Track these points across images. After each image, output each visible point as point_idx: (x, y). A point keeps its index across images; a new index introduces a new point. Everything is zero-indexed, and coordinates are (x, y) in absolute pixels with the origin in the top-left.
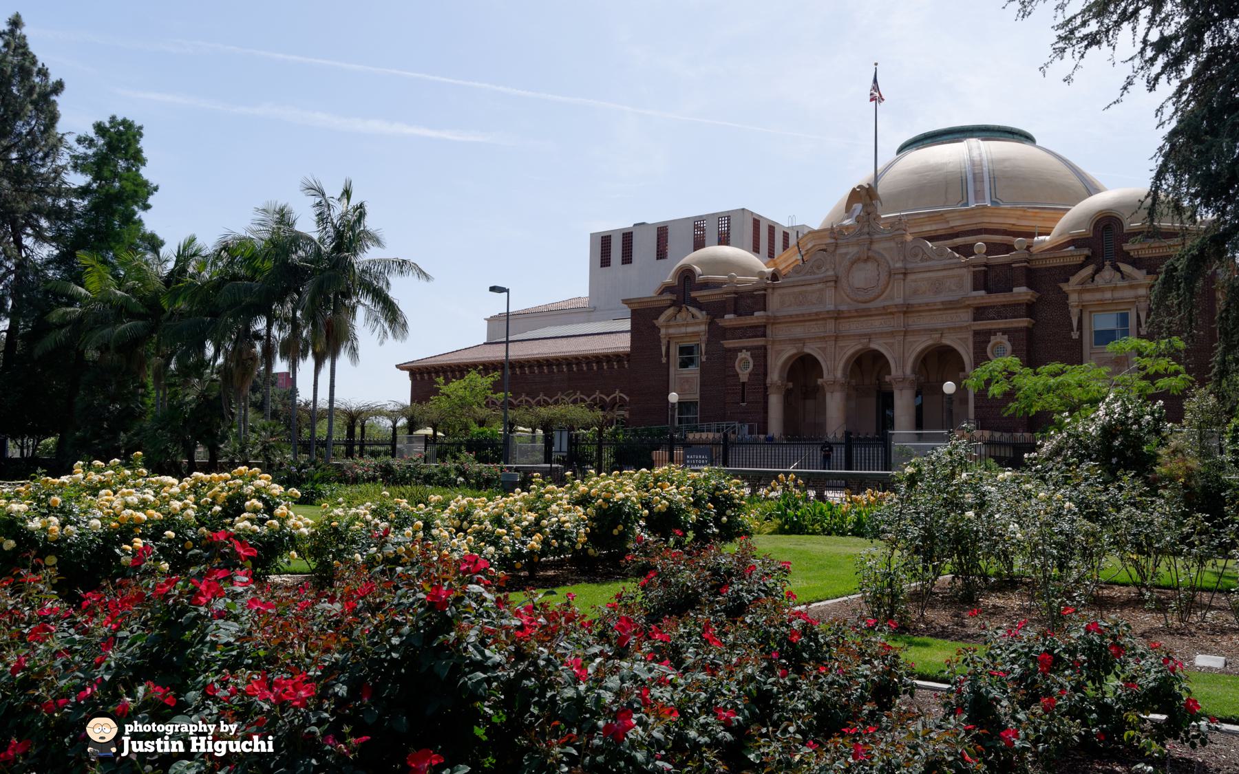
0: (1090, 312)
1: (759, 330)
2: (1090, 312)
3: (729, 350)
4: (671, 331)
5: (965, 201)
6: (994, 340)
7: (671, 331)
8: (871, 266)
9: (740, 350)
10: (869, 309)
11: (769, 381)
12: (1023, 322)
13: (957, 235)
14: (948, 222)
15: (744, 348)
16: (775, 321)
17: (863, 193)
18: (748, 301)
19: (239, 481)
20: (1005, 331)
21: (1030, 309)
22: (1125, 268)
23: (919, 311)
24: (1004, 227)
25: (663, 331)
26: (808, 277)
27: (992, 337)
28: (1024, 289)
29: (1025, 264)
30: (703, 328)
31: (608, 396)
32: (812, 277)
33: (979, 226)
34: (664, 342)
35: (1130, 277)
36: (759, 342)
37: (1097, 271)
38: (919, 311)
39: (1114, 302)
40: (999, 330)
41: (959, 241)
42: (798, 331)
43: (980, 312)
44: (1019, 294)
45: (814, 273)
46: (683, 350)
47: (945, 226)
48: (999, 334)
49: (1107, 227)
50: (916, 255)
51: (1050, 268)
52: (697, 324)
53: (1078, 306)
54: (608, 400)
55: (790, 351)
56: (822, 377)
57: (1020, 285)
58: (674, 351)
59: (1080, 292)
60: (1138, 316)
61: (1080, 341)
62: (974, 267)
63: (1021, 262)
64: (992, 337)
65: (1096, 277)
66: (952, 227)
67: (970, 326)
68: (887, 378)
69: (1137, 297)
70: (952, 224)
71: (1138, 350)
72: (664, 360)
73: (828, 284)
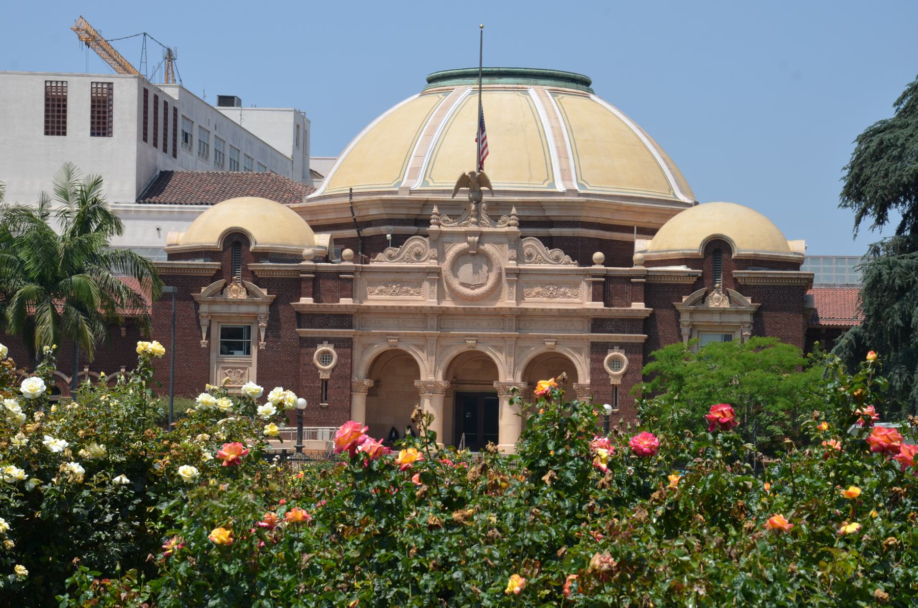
0: (699, 331)
1: (344, 319)
2: (699, 331)
4: (217, 308)
5: (550, 181)
7: (217, 308)
9: (321, 341)
13: (550, 223)
14: (544, 210)
15: (325, 339)
17: (473, 181)
19: (166, 442)
20: (622, 346)
21: (646, 324)
24: (600, 221)
25: (204, 309)
29: (644, 280)
30: (264, 309)
33: (576, 219)
39: (721, 325)
40: (617, 344)
41: (555, 231)
43: (598, 323)
45: (413, 261)
46: (227, 333)
47: (542, 214)
51: (664, 285)
52: (257, 304)
53: (688, 326)
57: (639, 301)
58: (216, 333)
59: (692, 313)
62: (593, 277)
63: (640, 278)
66: (548, 216)
69: (742, 323)
70: (548, 213)
71: (47, 215)
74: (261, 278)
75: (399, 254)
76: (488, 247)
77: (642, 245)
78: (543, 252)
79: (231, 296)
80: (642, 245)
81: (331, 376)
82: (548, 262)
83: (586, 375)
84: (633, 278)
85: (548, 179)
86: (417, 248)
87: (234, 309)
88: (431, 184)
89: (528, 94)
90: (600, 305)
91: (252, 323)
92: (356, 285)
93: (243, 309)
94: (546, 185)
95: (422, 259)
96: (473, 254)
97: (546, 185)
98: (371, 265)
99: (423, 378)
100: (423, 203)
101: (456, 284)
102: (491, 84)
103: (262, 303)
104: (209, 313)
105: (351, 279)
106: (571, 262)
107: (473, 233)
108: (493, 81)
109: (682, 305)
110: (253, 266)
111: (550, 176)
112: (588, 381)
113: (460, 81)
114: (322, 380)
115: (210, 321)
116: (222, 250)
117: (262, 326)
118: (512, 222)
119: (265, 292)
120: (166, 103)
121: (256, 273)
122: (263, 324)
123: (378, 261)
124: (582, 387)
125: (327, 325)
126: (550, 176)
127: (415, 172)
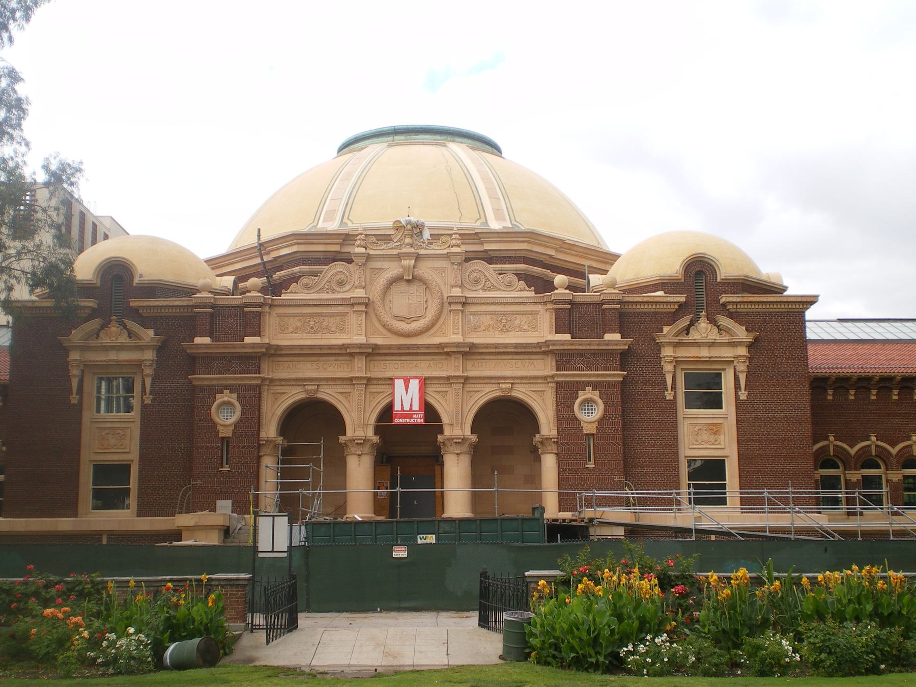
3: (202, 388)
5: (483, 220)
6: (582, 396)
8: (416, 290)
9: (581, 386)
10: (417, 347)
11: (263, 435)
12: (616, 375)
15: (226, 387)
16: (274, 353)
18: (231, 320)
20: (595, 386)
21: (624, 358)
22: (724, 321)
23: (482, 353)
25: (74, 356)
26: (324, 296)
27: (218, 396)
28: (617, 337)
30: (150, 355)
31: (852, 446)
32: (330, 296)
34: (75, 372)
35: (727, 331)
36: (250, 379)
37: (103, 327)
38: (482, 353)
42: (308, 370)
43: (564, 358)
44: (609, 343)
45: (333, 291)
48: (589, 389)
49: (699, 273)
50: (477, 281)
52: (140, 348)
54: (894, 451)
55: (295, 395)
56: (345, 434)
57: (614, 332)
60: (737, 379)
61: (674, 402)
62: (555, 304)
63: (613, 303)
64: (218, 396)
65: (102, 334)
67: (553, 376)
68: (440, 438)
72: (74, 399)
73: (357, 308)
74: (146, 317)
75: (317, 283)
76: (425, 270)
77: (595, 280)
78: (492, 276)
79: (105, 340)
80: (595, 280)
81: (234, 433)
82: (499, 289)
83: (552, 425)
84: (603, 304)
85: (480, 218)
86: (339, 276)
87: (113, 356)
88: (350, 224)
89: (448, 147)
90: (567, 337)
91: (135, 373)
92: (264, 321)
93: (125, 356)
94: (478, 224)
95: (344, 289)
96: (408, 281)
97: (478, 224)
98: (283, 297)
99: (350, 433)
100: (343, 237)
101: (387, 319)
102: (407, 140)
103: (148, 347)
104: (80, 361)
105: (260, 313)
106: (527, 289)
107: (408, 255)
108: (409, 137)
109: (665, 336)
110: (135, 303)
111: (482, 215)
112: (554, 432)
113: (375, 140)
114: (223, 438)
115: (83, 371)
116: (99, 285)
117: (148, 375)
118: (454, 242)
119: (151, 333)
120: (95, 226)
121: (141, 311)
122: (148, 371)
123: (291, 292)
124: (545, 441)
125: (229, 370)
126: (482, 215)
127: (330, 216)
